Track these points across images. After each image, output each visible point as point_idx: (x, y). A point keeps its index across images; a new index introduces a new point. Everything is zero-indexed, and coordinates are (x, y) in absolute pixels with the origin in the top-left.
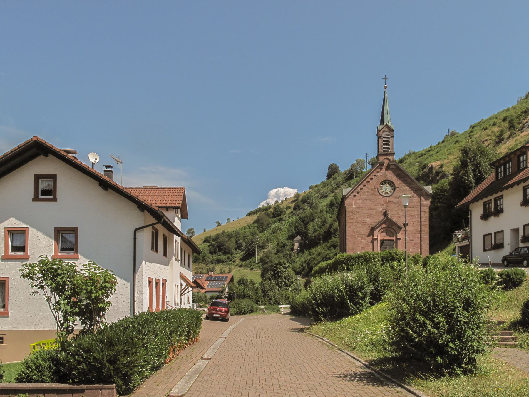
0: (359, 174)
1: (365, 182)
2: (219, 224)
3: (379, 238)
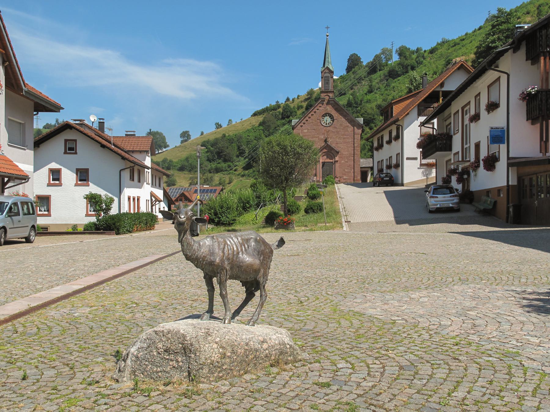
0: (383, 66)
1: (310, 115)
2: (218, 126)
3: (321, 161)
